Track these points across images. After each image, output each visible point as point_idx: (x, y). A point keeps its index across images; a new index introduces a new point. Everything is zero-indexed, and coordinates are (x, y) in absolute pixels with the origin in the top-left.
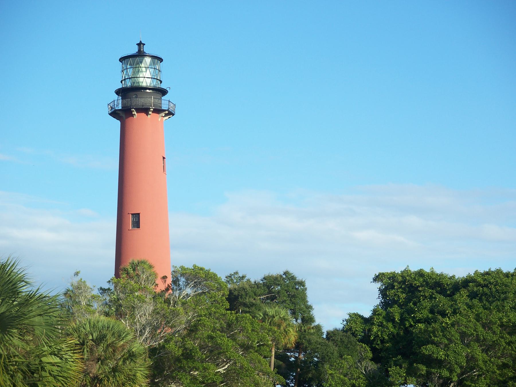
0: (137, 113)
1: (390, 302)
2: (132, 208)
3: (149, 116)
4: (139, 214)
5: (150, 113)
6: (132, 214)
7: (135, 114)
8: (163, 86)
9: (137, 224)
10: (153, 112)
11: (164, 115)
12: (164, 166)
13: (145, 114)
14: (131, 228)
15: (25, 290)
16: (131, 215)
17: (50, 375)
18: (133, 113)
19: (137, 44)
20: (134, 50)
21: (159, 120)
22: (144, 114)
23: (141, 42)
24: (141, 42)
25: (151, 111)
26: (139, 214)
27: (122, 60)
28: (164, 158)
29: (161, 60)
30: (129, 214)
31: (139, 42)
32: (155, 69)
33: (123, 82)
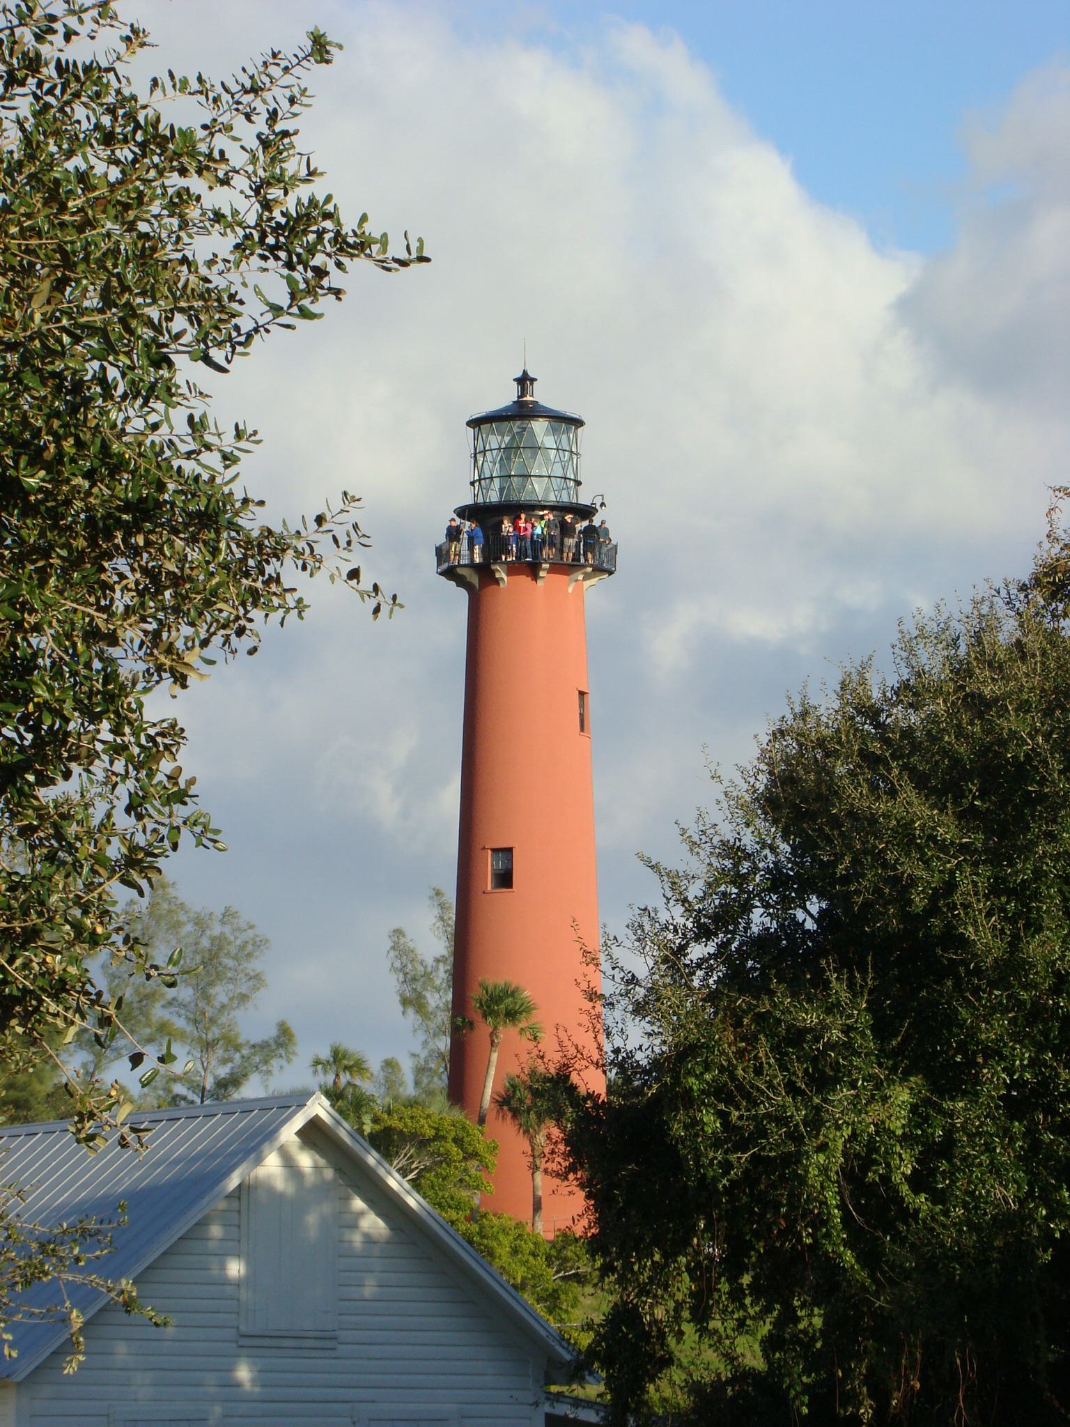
0: (508, 575)
1: (808, 976)
2: (493, 835)
3: (540, 583)
4: (510, 850)
5: (542, 574)
6: (494, 850)
7: (502, 579)
8: (585, 499)
9: (505, 879)
10: (550, 571)
11: (581, 577)
12: (582, 716)
13: (529, 579)
14: (489, 888)
15: (252, 523)
16: (490, 852)
17: (170, 356)
18: (497, 575)
19: (515, 380)
20: (506, 396)
21: (570, 590)
22: (524, 577)
23: (525, 373)
24: (525, 373)
25: (544, 570)
26: (510, 850)
27: (476, 423)
28: (582, 694)
29: (578, 423)
30: (484, 848)
31: (519, 374)
32: (558, 449)
33: (477, 484)
